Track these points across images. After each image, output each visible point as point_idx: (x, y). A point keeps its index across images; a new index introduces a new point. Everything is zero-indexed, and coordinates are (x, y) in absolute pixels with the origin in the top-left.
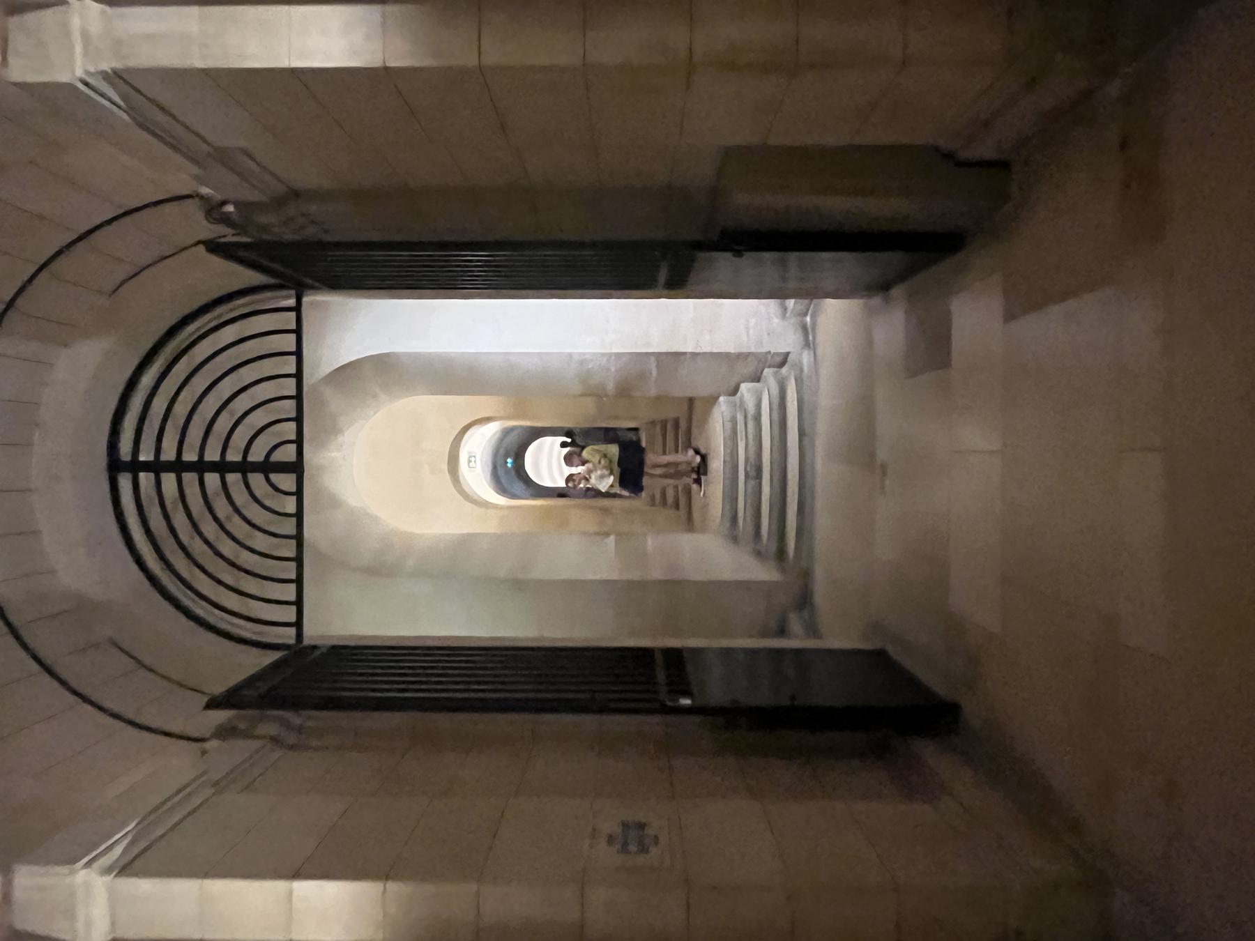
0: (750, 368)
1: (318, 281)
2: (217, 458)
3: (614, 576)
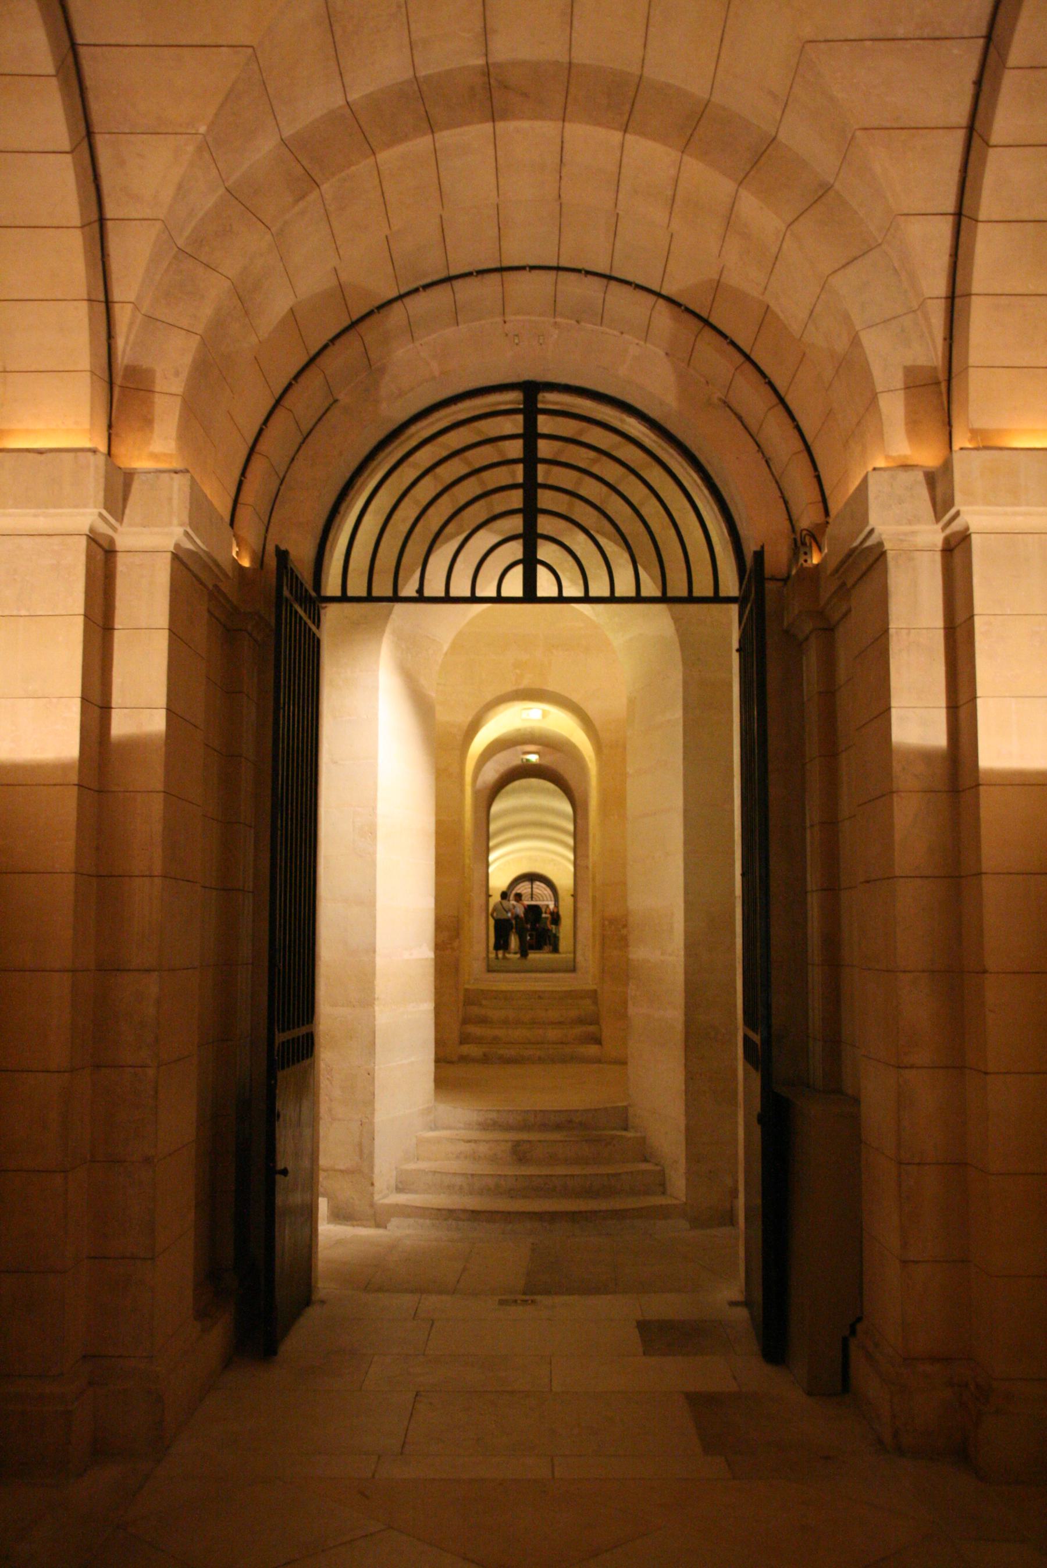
3: (380, 962)
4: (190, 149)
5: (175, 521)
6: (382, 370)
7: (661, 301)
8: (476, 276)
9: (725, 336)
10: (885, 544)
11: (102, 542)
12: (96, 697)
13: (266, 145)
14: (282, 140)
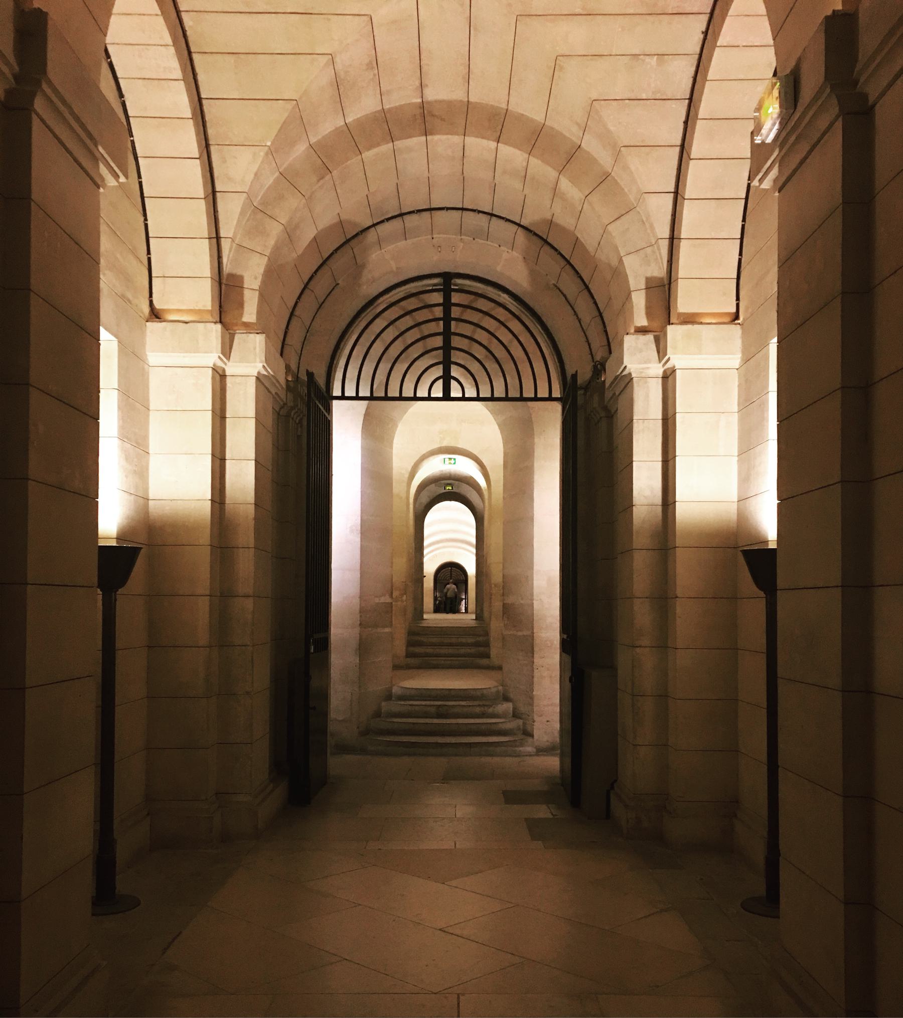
0: (522, 709)
1: (565, 417)
2: (453, 301)
4: (262, 154)
5: (258, 360)
6: (363, 266)
7: (520, 229)
8: (416, 213)
9: (556, 250)
10: (633, 374)
11: (219, 371)
12: (218, 455)
13: (301, 148)
14: (310, 145)
